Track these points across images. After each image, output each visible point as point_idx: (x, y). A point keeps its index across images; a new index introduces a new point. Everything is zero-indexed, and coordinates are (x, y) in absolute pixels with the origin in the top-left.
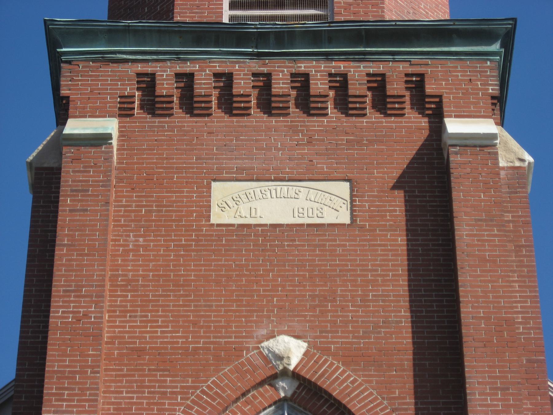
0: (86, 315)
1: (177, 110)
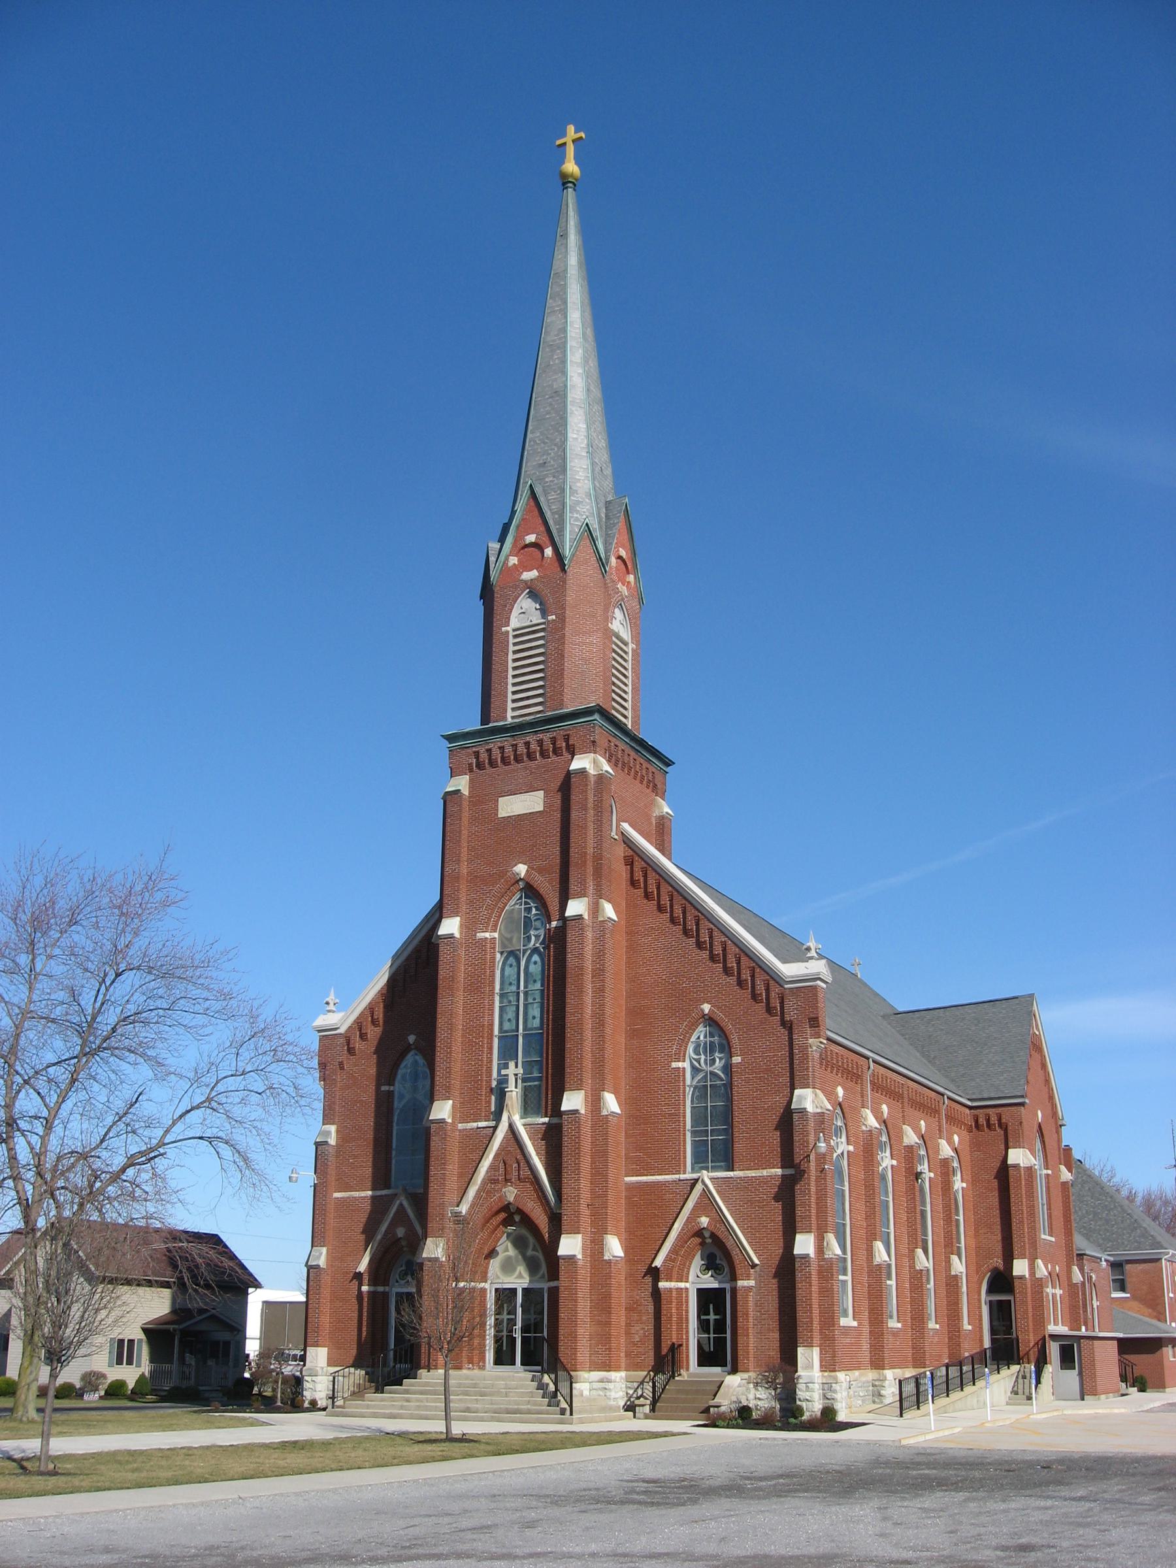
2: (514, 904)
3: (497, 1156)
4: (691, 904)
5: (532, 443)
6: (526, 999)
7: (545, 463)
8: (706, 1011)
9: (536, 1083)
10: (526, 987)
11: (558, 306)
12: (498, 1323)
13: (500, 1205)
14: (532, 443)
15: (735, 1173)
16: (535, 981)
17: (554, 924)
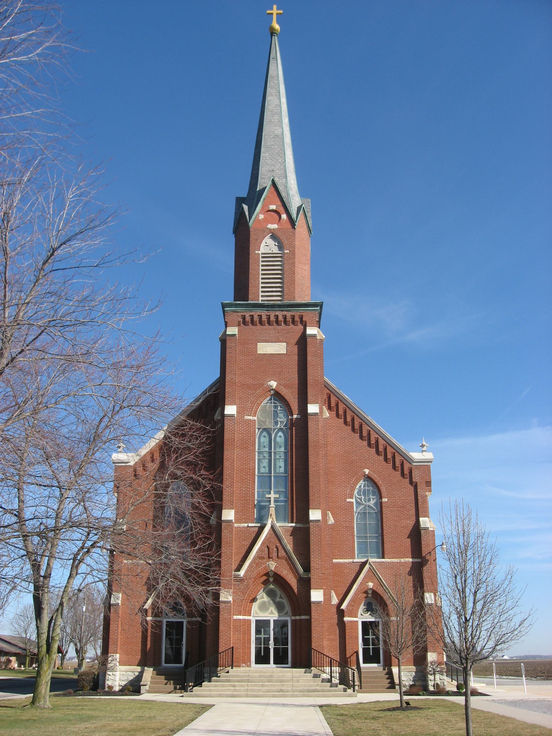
0: (233, 378)
1: (250, 324)
2: (266, 403)
3: (263, 543)
4: (357, 416)
5: (264, 158)
6: (275, 456)
7: (273, 170)
8: (367, 473)
9: (283, 504)
10: (275, 449)
11: (275, 93)
12: (258, 640)
13: (265, 572)
14: (264, 158)
15: (386, 559)
16: (280, 447)
17: (295, 416)
